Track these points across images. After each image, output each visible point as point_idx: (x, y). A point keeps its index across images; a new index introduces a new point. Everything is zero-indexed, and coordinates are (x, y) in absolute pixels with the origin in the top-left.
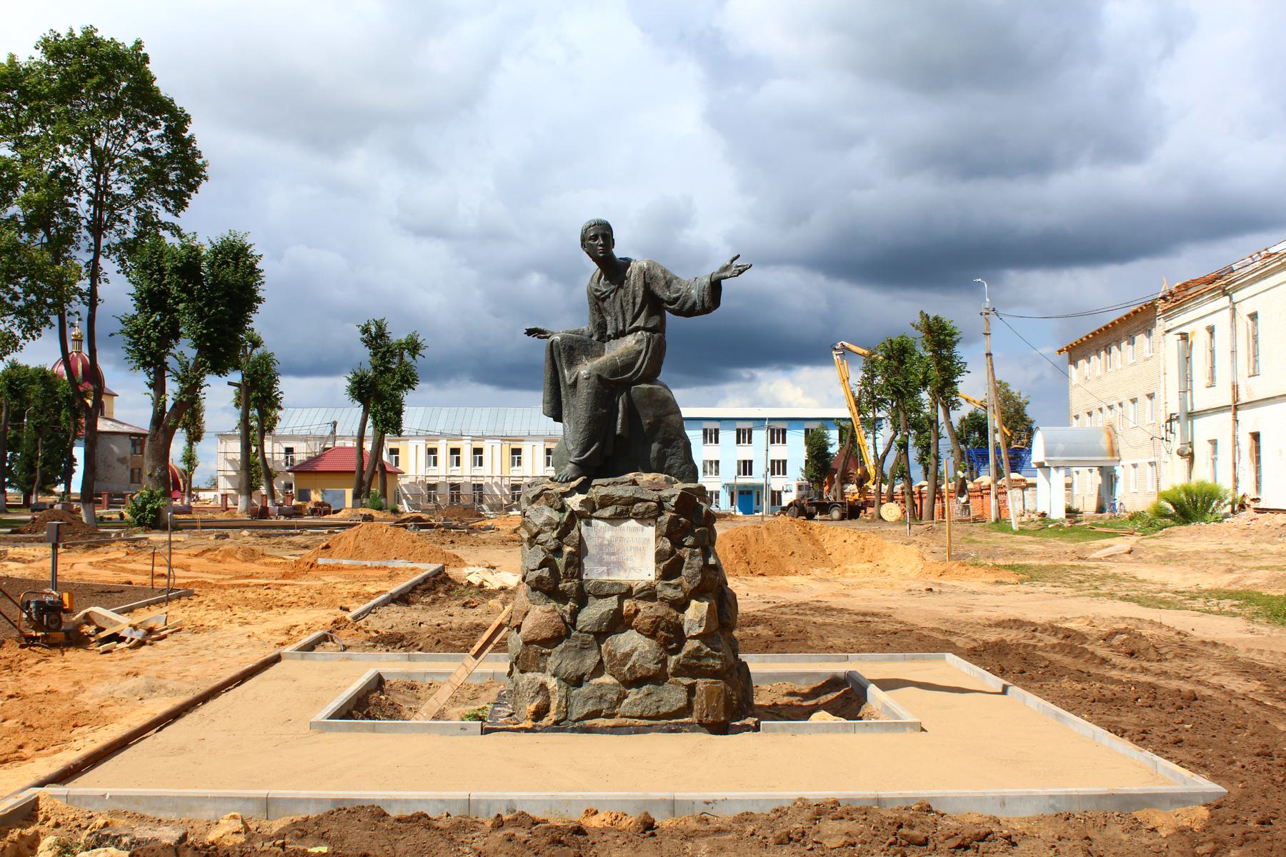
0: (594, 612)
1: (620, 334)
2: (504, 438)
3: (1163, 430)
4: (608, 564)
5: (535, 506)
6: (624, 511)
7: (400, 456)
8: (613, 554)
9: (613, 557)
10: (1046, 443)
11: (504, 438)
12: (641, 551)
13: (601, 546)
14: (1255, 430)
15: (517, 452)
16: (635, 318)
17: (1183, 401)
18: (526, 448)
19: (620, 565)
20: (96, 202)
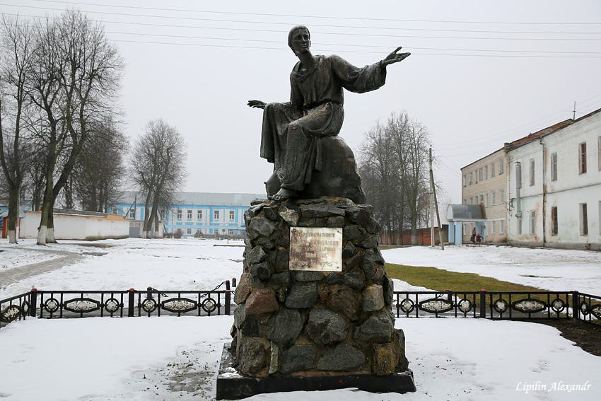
0: (298, 294)
1: (313, 105)
2: (210, 207)
3: (508, 206)
4: (309, 259)
5: (257, 218)
6: (324, 221)
7: (109, 317)
8: (313, 252)
9: (308, 253)
10: (454, 210)
11: (210, 207)
12: (332, 250)
13: (304, 247)
14: (584, 202)
15: (217, 212)
16: (325, 93)
17: (518, 193)
18: (221, 211)
19: (316, 260)
20: (94, 192)
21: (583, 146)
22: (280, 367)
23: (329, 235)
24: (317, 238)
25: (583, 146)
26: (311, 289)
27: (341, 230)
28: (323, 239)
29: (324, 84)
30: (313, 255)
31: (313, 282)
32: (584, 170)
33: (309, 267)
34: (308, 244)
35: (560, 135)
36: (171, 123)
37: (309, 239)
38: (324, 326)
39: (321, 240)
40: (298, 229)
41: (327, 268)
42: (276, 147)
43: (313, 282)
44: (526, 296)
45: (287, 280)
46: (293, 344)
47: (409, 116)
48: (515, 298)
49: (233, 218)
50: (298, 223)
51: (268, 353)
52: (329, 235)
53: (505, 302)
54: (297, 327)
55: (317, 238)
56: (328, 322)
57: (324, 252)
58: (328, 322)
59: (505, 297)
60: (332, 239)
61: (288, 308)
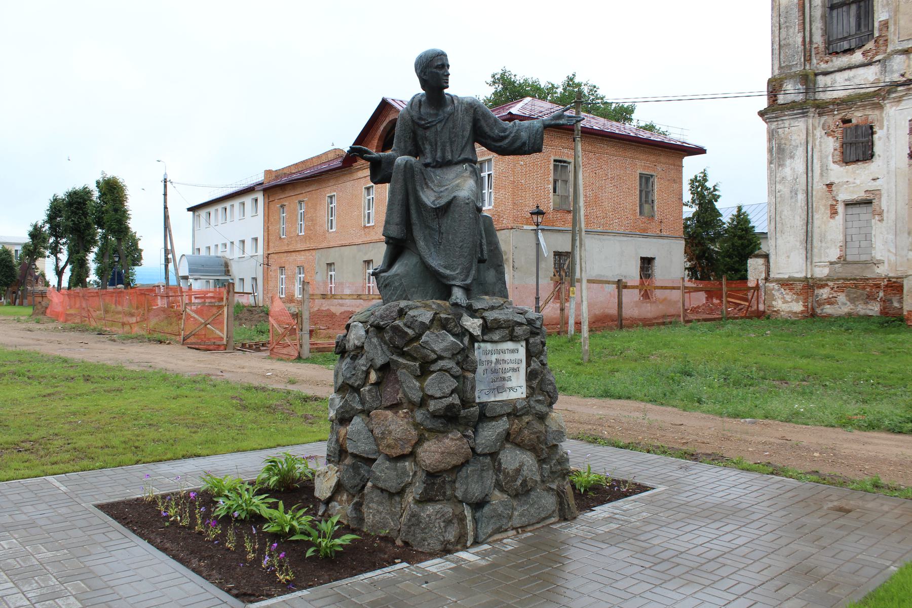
23: (513, 351)
26: (502, 425)
27: (524, 344)
29: (463, 137)
31: (503, 415)
35: (506, 254)
36: (109, 175)
37: (494, 358)
38: (518, 471)
41: (513, 395)
42: (893, 195)
43: (503, 415)
45: (64, 240)
46: (488, 502)
51: (462, 519)
52: (513, 351)
54: (490, 479)
56: (522, 465)
58: (522, 465)
61: (479, 455)
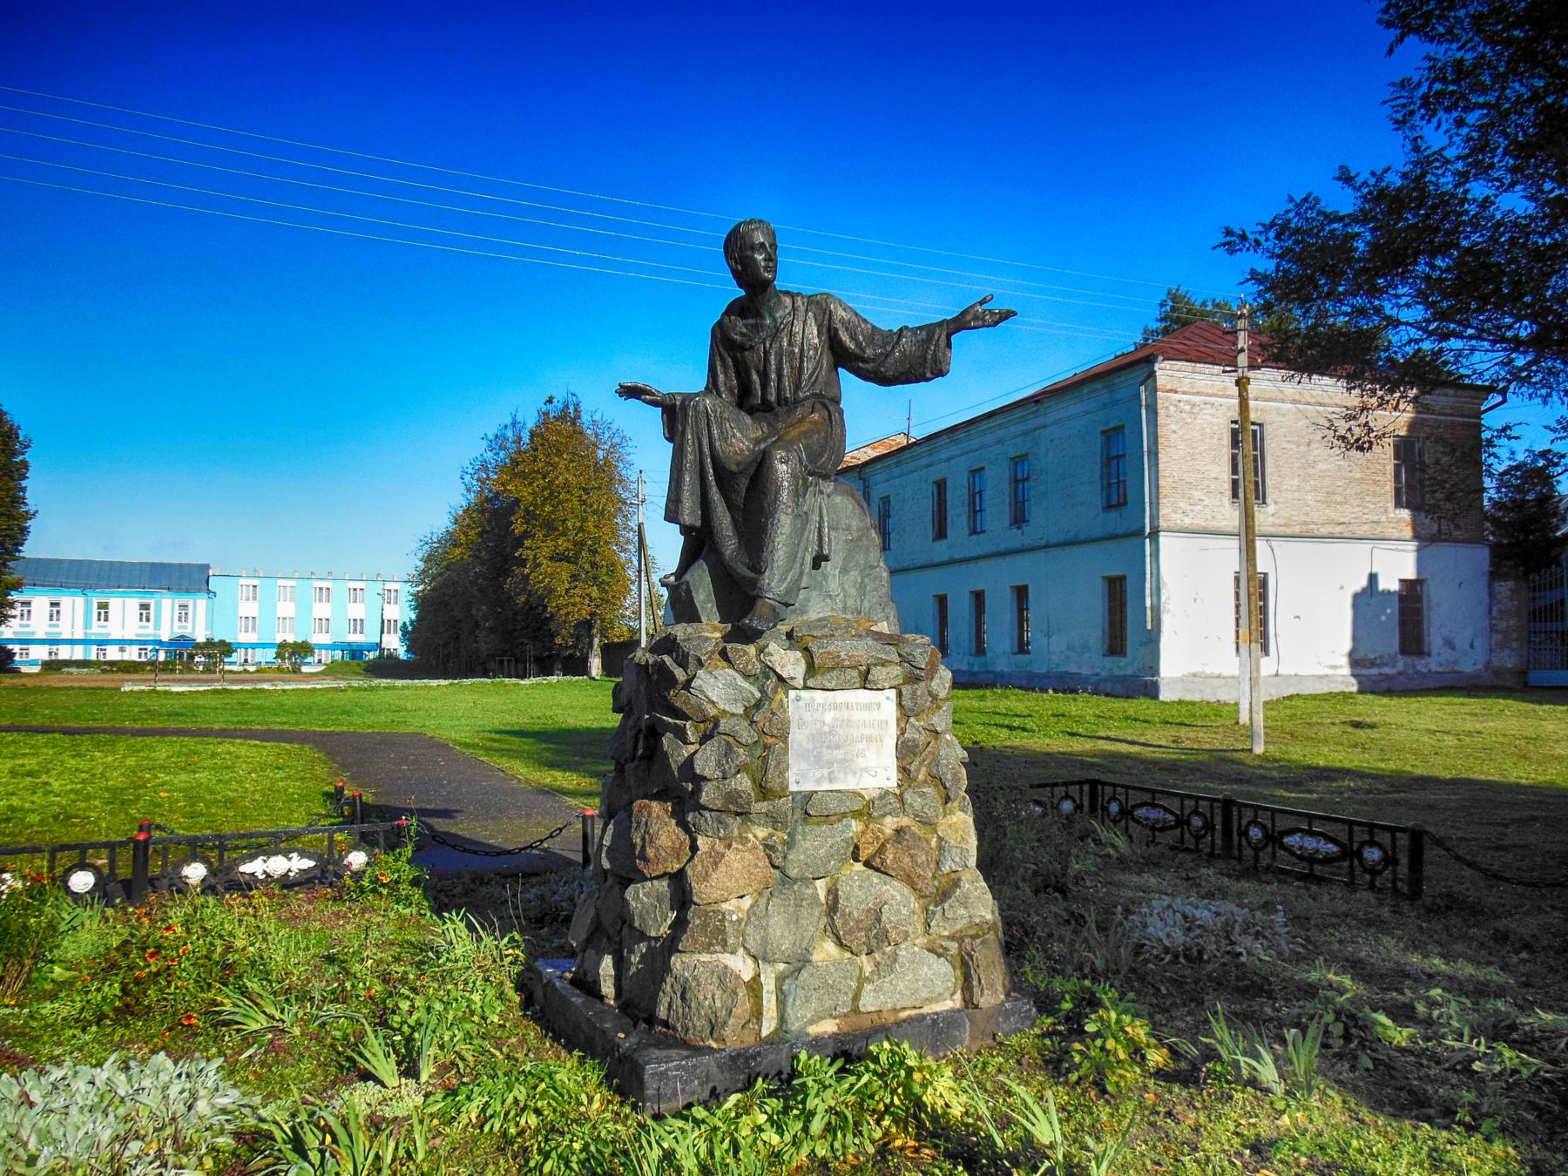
4: (831, 763)
8: (838, 747)
19: (845, 764)
21: (941, 486)
22: (782, 1019)
23: (869, 707)
24: (846, 714)
25: (941, 486)
28: (857, 715)
30: (838, 754)
32: (941, 533)
33: (831, 781)
34: (826, 729)
37: (829, 717)
39: (854, 718)
40: (805, 694)
44: (1147, 798)
47: (583, 407)
48: (1282, 823)
49: (148, 620)
50: (805, 680)
53: (1074, 800)
55: (846, 714)
57: (860, 746)
59: (1385, 838)
60: (875, 715)
61: (795, 881)
